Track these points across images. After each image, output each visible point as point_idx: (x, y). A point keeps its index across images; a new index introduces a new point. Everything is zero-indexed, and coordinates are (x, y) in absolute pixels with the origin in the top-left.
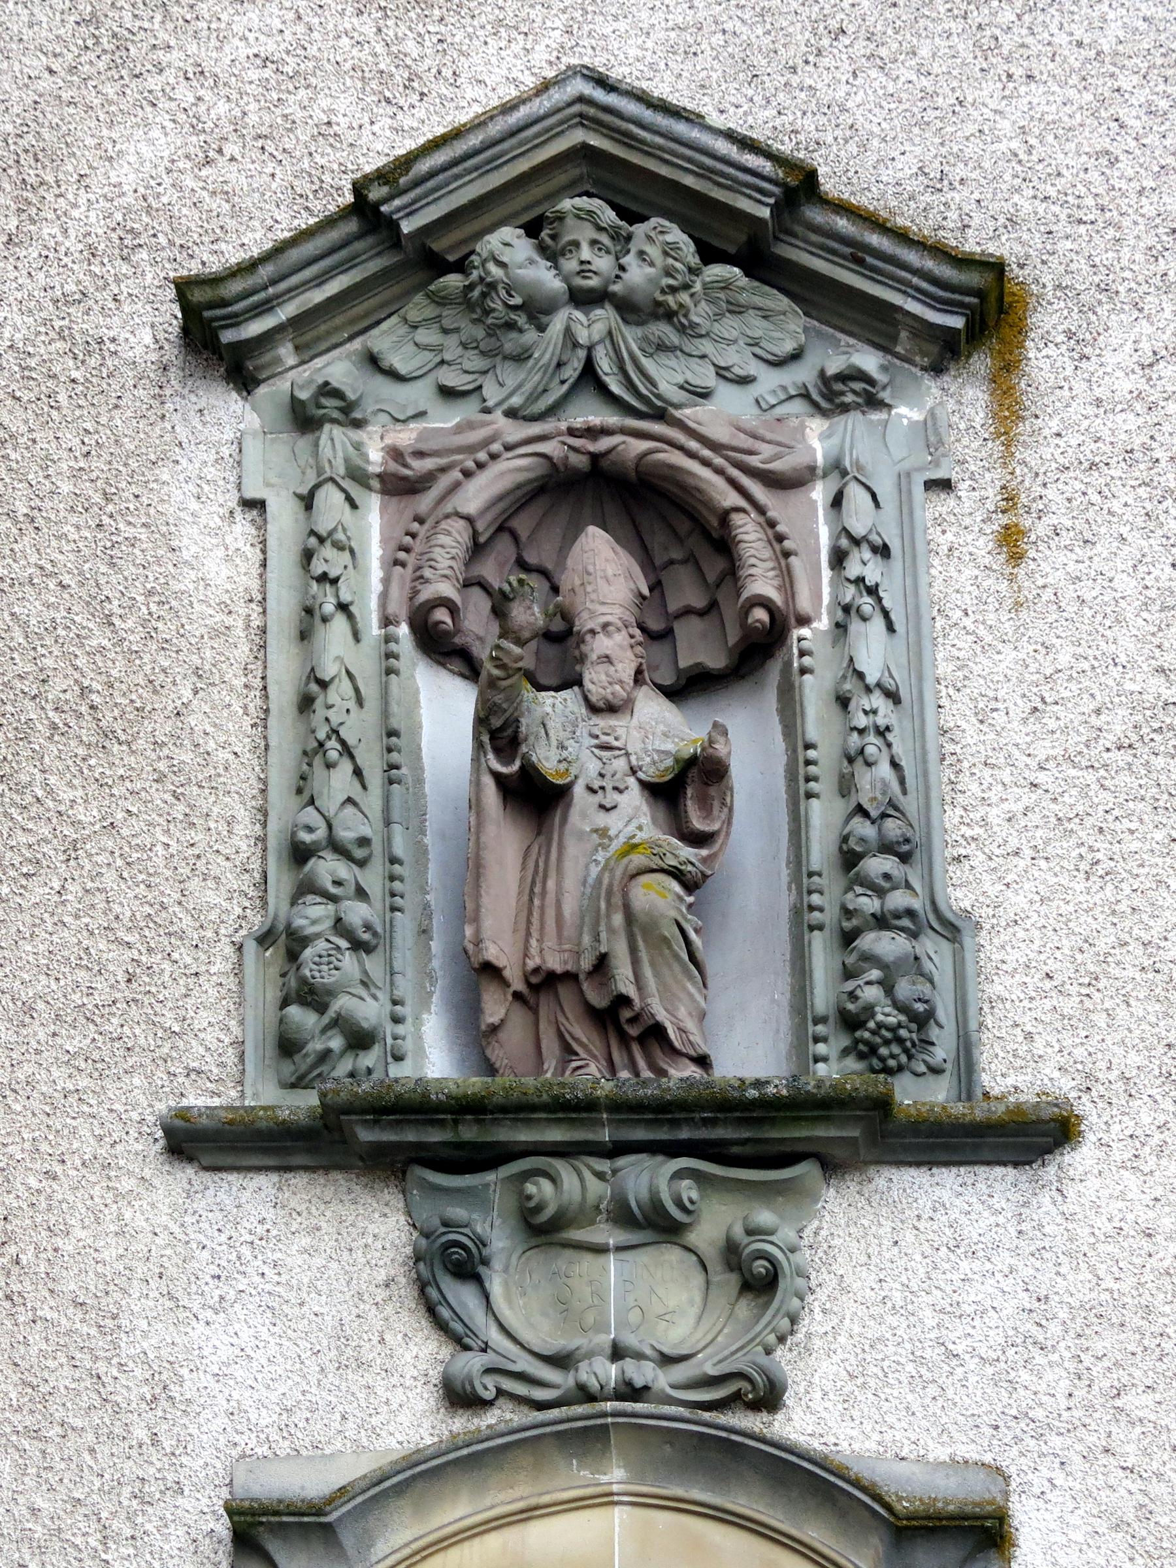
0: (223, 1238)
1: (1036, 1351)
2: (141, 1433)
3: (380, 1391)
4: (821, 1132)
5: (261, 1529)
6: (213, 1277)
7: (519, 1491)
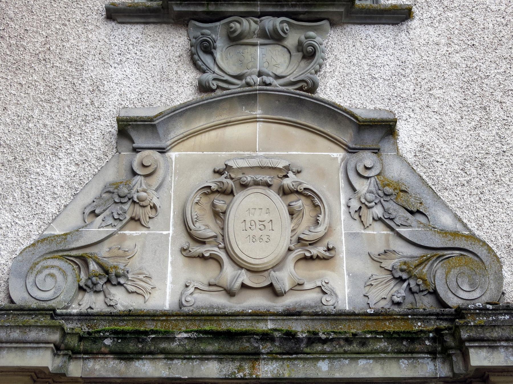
0: (123, 43)
1: (402, 77)
2: (87, 101)
3: (175, 88)
4: (331, 9)
5: (129, 127)
6: (118, 54)
7: (224, 117)
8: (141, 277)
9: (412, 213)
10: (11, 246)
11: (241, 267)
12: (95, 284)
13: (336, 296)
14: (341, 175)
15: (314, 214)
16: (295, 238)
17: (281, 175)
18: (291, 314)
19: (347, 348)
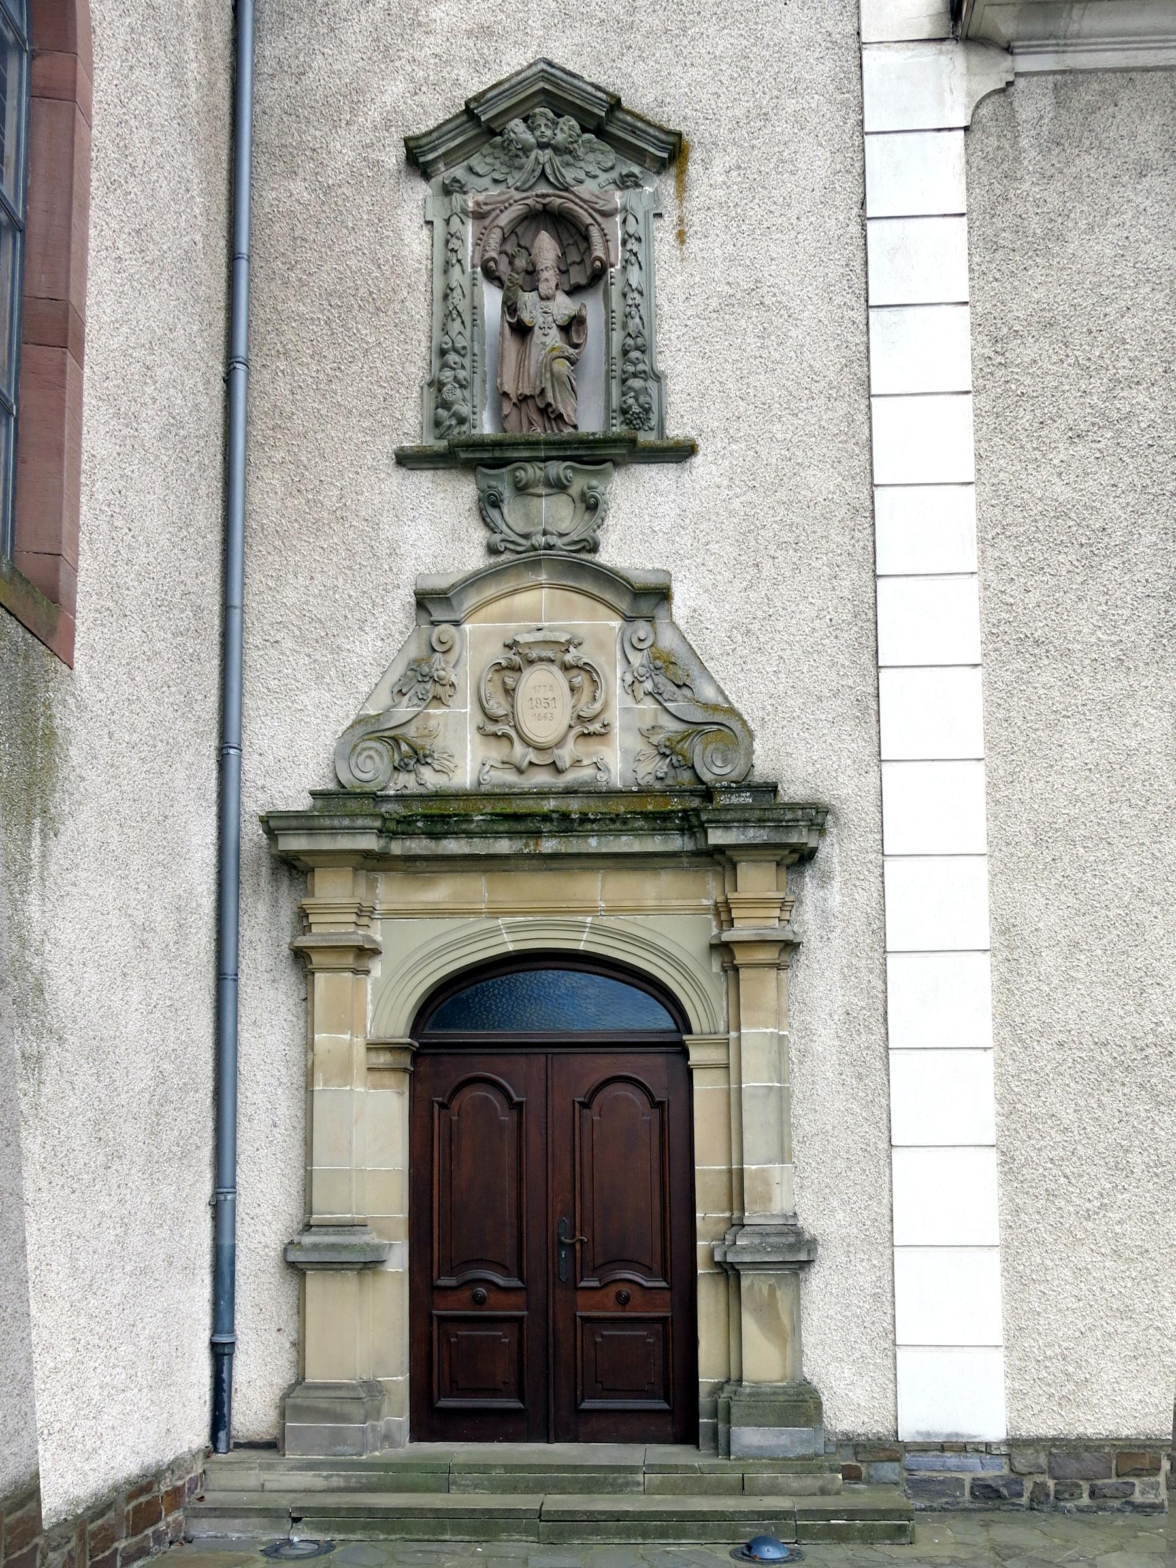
2: (386, 567)
4: (613, 451)
8: (445, 756)
9: (678, 686)
10: (334, 727)
11: (529, 745)
12: (407, 765)
13: (609, 770)
14: (618, 646)
15: (592, 689)
16: (575, 715)
17: (563, 649)
18: (569, 792)
19: (612, 827)
